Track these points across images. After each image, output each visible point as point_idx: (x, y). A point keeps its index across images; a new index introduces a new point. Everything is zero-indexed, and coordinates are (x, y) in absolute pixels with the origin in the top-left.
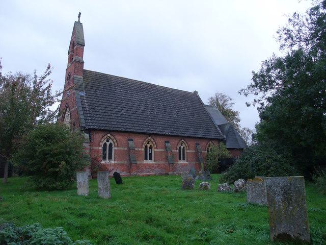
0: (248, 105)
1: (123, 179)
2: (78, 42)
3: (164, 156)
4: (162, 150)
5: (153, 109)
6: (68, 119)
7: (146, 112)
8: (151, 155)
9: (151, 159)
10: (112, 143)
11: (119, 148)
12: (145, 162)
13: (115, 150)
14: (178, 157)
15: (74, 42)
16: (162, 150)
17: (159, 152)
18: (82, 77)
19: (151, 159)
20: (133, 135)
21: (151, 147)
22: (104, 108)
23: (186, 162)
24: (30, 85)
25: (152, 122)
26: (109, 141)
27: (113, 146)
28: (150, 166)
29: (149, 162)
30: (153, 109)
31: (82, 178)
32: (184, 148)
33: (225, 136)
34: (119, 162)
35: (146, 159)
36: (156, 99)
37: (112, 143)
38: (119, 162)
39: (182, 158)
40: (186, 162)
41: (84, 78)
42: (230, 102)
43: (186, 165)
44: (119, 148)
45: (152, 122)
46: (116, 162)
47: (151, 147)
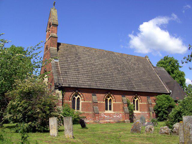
0: (59, 44)
1: (86, 125)
3: (121, 108)
4: (146, 103)
5: (111, 70)
6: (46, 80)
7: (106, 73)
8: (110, 106)
9: (110, 109)
10: (138, 100)
11: (143, 103)
12: (106, 112)
13: (140, 105)
15: (50, 23)
16: (146, 103)
19: (110, 109)
21: (110, 100)
22: (73, 71)
23: (113, 112)
25: (111, 81)
27: (80, 100)
28: (109, 115)
29: (108, 112)
30: (111, 70)
31: (53, 122)
32: (137, 100)
33: (171, 91)
35: (107, 109)
37: (112, 99)
40: (113, 112)
44: (143, 103)
45: (111, 81)
47: (110, 100)
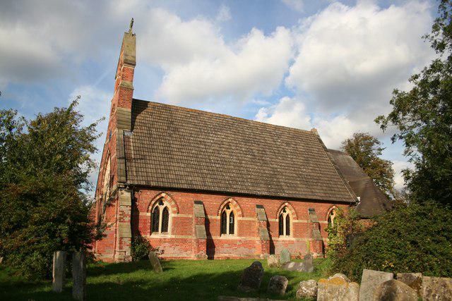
2: (126, 60)
8: (232, 226)
9: (232, 231)
14: (278, 230)
17: (247, 221)
18: (130, 110)
20: (203, 196)
21: (232, 214)
24: (273, 33)
26: (163, 204)
28: (232, 243)
33: (359, 198)
34: (178, 237)
36: (247, 141)
38: (178, 237)
39: (131, 67)
41: (60, 250)
42: (375, 146)
43: (292, 242)
46: (174, 237)
